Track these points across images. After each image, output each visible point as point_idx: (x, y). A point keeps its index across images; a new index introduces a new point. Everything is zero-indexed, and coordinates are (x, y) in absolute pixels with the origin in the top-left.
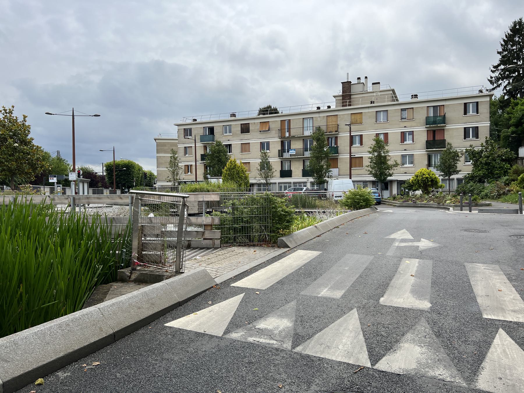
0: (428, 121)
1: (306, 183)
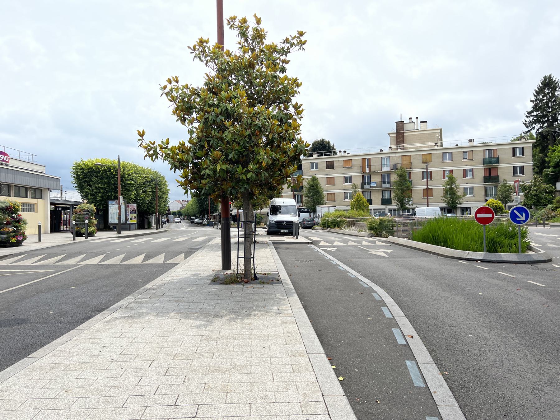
0: (485, 161)
1: (385, 209)
